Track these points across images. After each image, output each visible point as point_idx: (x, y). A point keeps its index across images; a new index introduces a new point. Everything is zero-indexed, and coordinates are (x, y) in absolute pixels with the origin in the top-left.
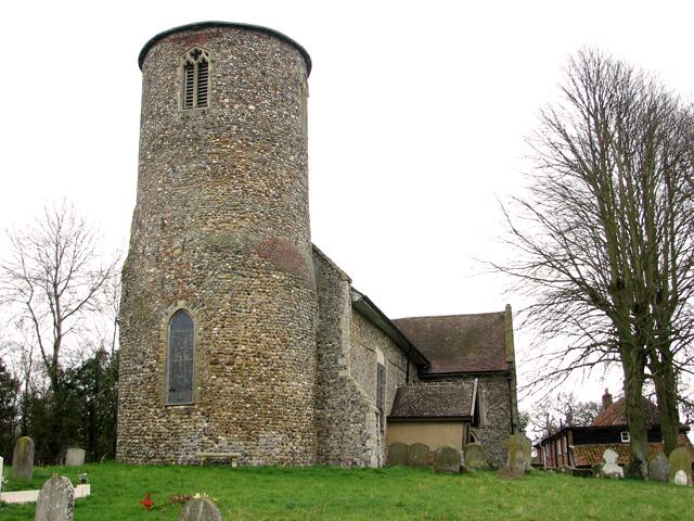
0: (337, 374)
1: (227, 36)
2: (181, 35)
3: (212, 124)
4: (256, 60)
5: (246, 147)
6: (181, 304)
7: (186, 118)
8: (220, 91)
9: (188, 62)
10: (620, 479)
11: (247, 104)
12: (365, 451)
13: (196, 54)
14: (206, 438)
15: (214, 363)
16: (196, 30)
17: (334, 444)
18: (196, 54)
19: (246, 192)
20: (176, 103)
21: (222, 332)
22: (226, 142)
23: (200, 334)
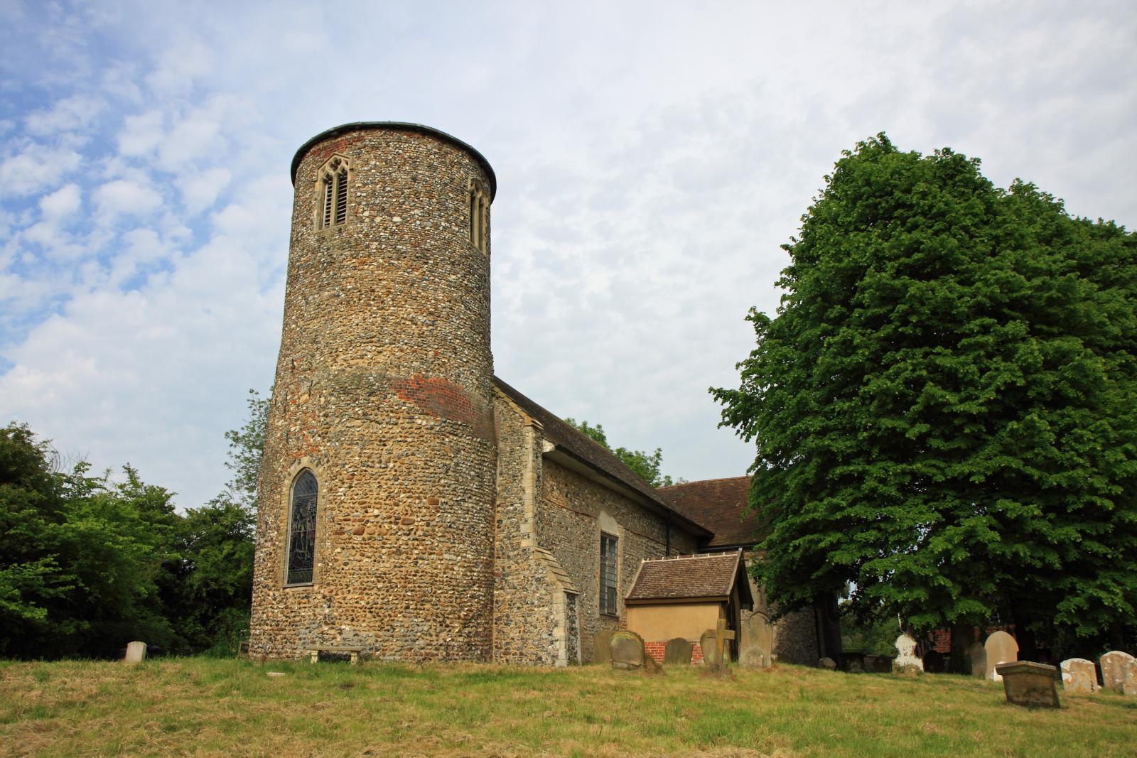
0: (519, 544)
1: (370, 138)
2: (321, 146)
3: (349, 242)
4: (404, 165)
5: (390, 268)
6: (305, 461)
7: (322, 240)
8: (360, 204)
9: (328, 176)
10: (919, 673)
11: (391, 216)
12: (552, 643)
13: (336, 165)
14: (326, 628)
15: (340, 532)
16: (336, 137)
17: (514, 633)
18: (336, 165)
19: (385, 320)
20: (312, 224)
21: (349, 493)
22: (364, 263)
23: (323, 497)
